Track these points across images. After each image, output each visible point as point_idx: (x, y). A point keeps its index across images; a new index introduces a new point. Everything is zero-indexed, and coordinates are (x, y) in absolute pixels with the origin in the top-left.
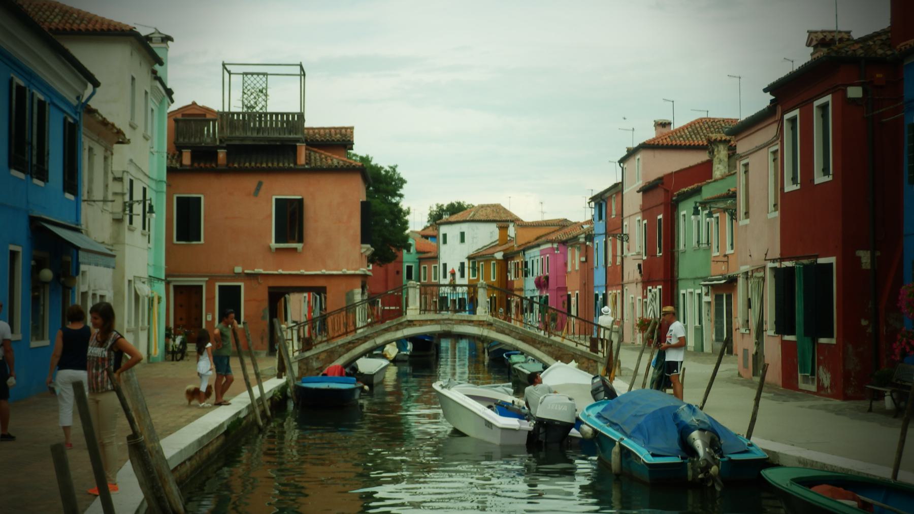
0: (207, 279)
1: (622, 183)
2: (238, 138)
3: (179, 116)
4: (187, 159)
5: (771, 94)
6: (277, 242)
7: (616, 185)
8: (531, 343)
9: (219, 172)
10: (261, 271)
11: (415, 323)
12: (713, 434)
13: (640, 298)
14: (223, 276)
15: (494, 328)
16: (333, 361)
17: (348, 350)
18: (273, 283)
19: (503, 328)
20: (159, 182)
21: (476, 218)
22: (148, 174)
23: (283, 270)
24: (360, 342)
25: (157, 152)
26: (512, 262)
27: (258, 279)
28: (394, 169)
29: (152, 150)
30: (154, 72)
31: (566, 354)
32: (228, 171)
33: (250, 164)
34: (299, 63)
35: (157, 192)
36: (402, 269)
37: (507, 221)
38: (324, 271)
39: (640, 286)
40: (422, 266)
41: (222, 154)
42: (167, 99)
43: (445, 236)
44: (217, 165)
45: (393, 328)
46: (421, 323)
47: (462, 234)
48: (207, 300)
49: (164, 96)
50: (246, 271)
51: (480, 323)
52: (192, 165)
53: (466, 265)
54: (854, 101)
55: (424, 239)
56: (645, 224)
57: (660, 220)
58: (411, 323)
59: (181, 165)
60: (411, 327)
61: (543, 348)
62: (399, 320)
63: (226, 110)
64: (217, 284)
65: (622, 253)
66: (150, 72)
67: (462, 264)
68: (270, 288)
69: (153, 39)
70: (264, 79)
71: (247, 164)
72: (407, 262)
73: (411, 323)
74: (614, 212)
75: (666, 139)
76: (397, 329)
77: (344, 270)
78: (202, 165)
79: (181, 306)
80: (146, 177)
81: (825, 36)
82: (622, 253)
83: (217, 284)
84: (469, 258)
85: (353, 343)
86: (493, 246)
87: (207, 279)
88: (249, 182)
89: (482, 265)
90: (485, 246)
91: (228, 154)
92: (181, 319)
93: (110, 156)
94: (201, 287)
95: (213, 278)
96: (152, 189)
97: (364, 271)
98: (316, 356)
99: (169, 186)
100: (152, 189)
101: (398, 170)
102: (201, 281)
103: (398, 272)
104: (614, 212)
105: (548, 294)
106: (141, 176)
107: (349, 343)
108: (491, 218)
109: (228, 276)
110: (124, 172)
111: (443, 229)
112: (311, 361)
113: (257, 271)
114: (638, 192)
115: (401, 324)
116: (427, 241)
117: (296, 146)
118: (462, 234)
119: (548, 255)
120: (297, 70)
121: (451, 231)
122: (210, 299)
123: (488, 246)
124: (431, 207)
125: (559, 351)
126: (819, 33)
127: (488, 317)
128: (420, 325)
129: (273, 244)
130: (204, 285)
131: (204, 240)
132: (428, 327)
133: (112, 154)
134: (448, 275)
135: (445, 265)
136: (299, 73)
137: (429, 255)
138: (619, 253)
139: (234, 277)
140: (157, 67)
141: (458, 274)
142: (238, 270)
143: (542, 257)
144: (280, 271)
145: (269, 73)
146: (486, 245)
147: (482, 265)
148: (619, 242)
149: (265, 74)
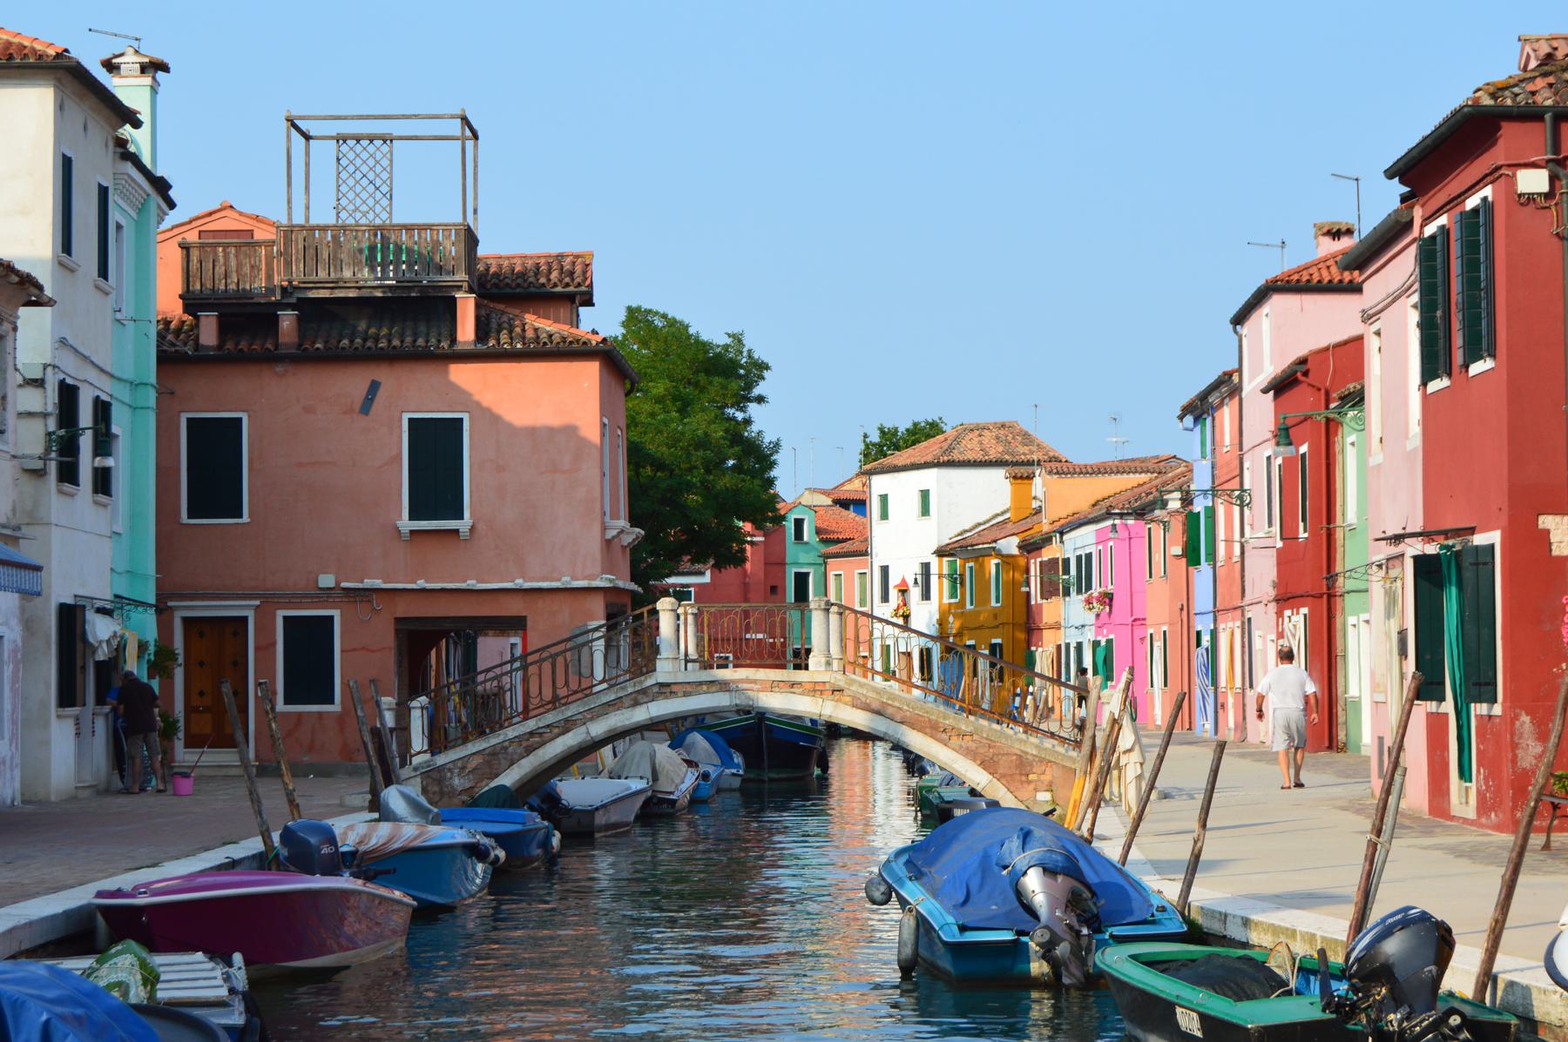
0: (257, 602)
1: (1240, 370)
2: (319, 284)
3: (192, 237)
4: (209, 333)
5: (1402, 182)
6: (414, 516)
7: (1229, 375)
8: (928, 730)
9: (272, 358)
10: (378, 583)
11: (674, 688)
12: (1076, 884)
13: (1274, 637)
14: (294, 596)
15: (848, 699)
16: (497, 775)
17: (529, 750)
18: (405, 609)
19: (867, 698)
20: (135, 385)
21: (956, 456)
22: (108, 369)
23: (427, 582)
24: (556, 731)
25: (132, 319)
26: (1039, 560)
27: (370, 602)
28: (738, 339)
29: (118, 316)
30: (121, 143)
31: (1003, 755)
32: (303, 357)
33: (352, 342)
34: (459, 112)
35: (134, 408)
36: (784, 578)
37: (1030, 463)
38: (520, 583)
39: (1273, 607)
40: (831, 575)
41: (287, 321)
42: (156, 199)
43: (884, 499)
44: (277, 346)
45: (627, 702)
46: (689, 689)
47: (925, 495)
48: (257, 648)
49: (148, 195)
50: (344, 585)
51: (816, 689)
52: (220, 347)
53: (934, 569)
54: (1530, 198)
55: (838, 509)
56: (1280, 466)
57: (1303, 456)
58: (665, 689)
59: (197, 346)
60: (666, 698)
61: (955, 741)
62: (641, 683)
63: (299, 219)
64: (281, 614)
65: (1242, 534)
66: (111, 144)
67: (926, 567)
68: (398, 620)
69: (122, 66)
70: (385, 148)
71: (243, 345)
72: (796, 564)
73: (665, 689)
74: (1227, 441)
75: (1328, 267)
76: (636, 704)
77: (566, 579)
78: (243, 345)
79: (201, 664)
80: (104, 377)
81: (1556, 49)
82: (1242, 534)
83: (281, 614)
84: (941, 553)
85: (541, 734)
86: (1000, 527)
87: (257, 602)
88: (352, 382)
89: (971, 568)
90: (980, 524)
91: (300, 319)
92: (201, 694)
93: (11, 333)
94: (245, 619)
95: (269, 600)
96: (123, 403)
97: (611, 581)
98: (460, 764)
99: (161, 393)
100: (123, 403)
101: (748, 343)
102: (246, 609)
103: (774, 589)
104: (1227, 441)
105: (1111, 636)
106: (92, 375)
107: (532, 734)
108: (993, 455)
109: (305, 596)
110: (45, 367)
111: (880, 483)
112: (449, 775)
113: (369, 583)
114: (1265, 391)
115: (644, 691)
116: (844, 512)
117: (454, 299)
118: (925, 495)
119: (1111, 543)
120: (455, 127)
121: (898, 488)
122: (265, 648)
123: (985, 523)
124: (866, 436)
125: (990, 747)
126: (1542, 42)
127: (835, 678)
128: (686, 694)
129: (406, 524)
130: (250, 614)
131: (250, 516)
132: (703, 697)
133: (15, 329)
134: (893, 594)
135: (885, 570)
136: (459, 133)
137: (847, 546)
138: (1237, 535)
139: (316, 596)
140: (127, 131)
141: (915, 593)
142: (327, 581)
143: (1100, 547)
144: (421, 584)
145: (395, 134)
146: (981, 521)
147: (971, 568)
148: (1236, 509)
149: (387, 139)
